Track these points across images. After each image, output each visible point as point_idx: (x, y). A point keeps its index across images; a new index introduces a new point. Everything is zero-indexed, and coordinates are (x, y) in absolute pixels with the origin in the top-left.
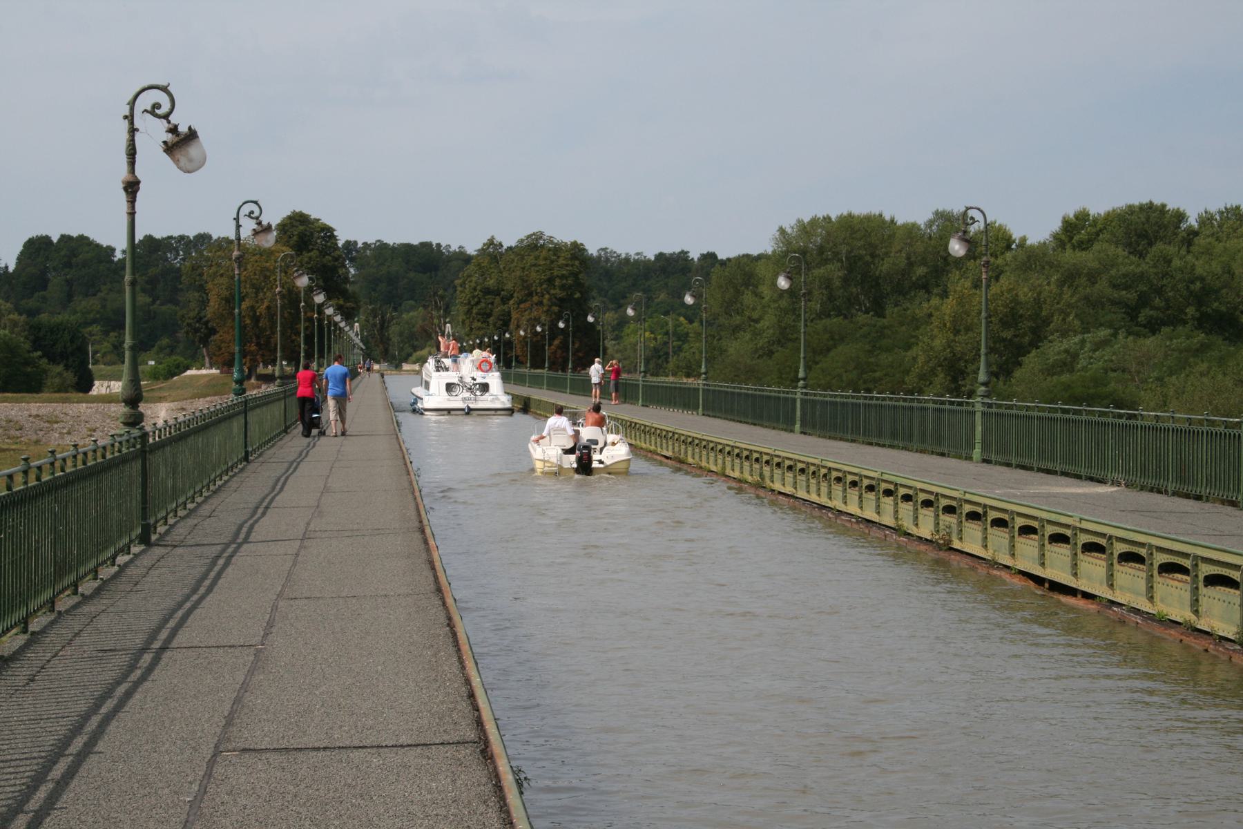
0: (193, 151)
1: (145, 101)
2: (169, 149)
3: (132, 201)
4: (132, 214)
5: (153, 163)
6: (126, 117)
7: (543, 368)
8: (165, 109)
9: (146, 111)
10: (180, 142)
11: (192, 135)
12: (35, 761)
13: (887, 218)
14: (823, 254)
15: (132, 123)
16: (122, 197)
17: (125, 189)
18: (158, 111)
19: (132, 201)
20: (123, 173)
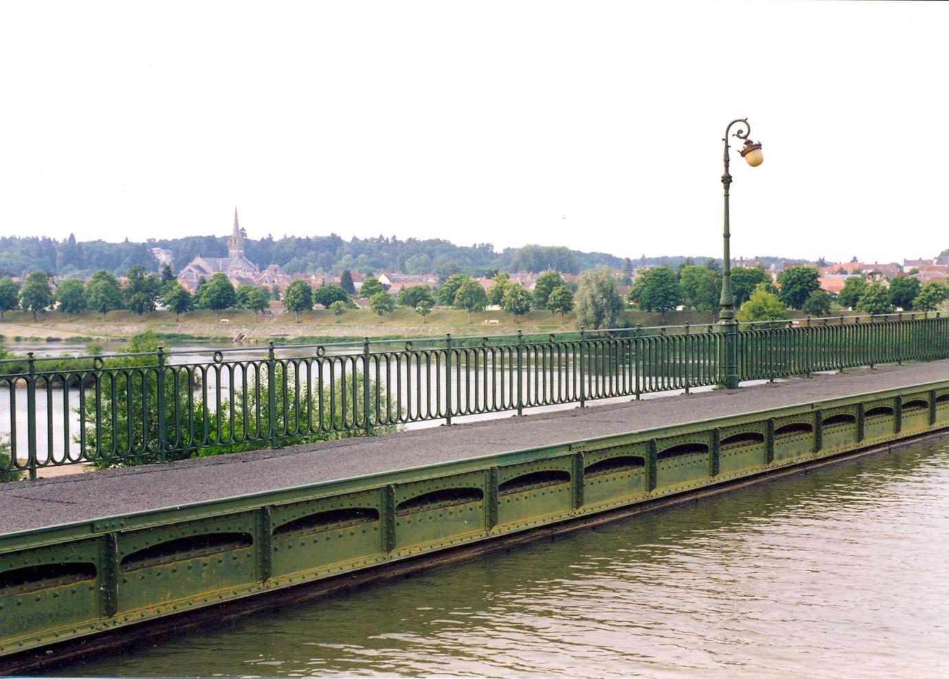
1: (734, 130)
2: (743, 154)
3: (727, 188)
4: (727, 196)
5: (739, 165)
11: (759, 146)
15: (727, 142)
19: (727, 188)
20: (723, 172)
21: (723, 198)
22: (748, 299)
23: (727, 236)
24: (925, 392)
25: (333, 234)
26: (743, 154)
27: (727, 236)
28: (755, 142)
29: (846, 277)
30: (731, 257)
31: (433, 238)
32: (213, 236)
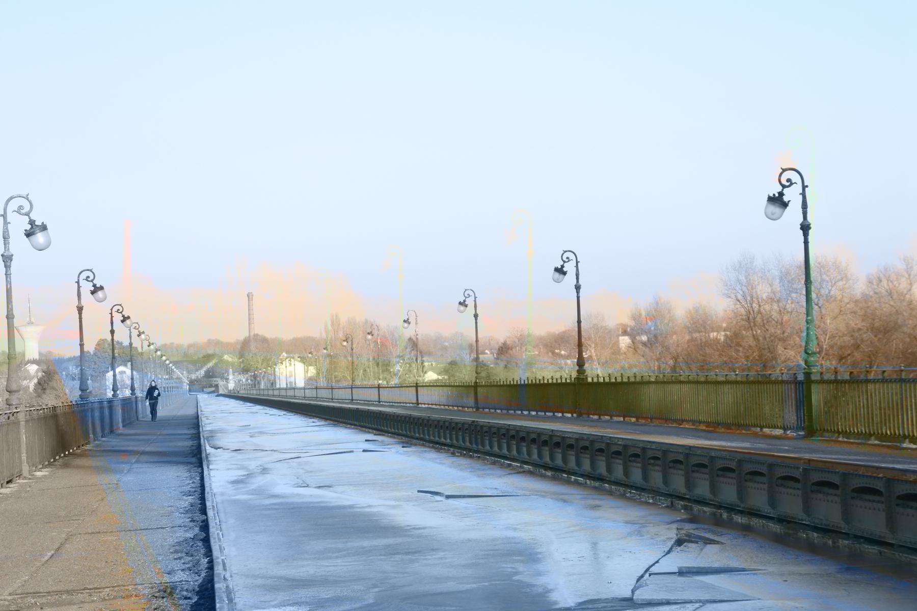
1: (115, 309)
2: (93, 293)
3: (806, 235)
8: (27, 208)
10: (96, 290)
11: (102, 288)
17: (801, 228)
20: (14, 264)
28: (565, 269)
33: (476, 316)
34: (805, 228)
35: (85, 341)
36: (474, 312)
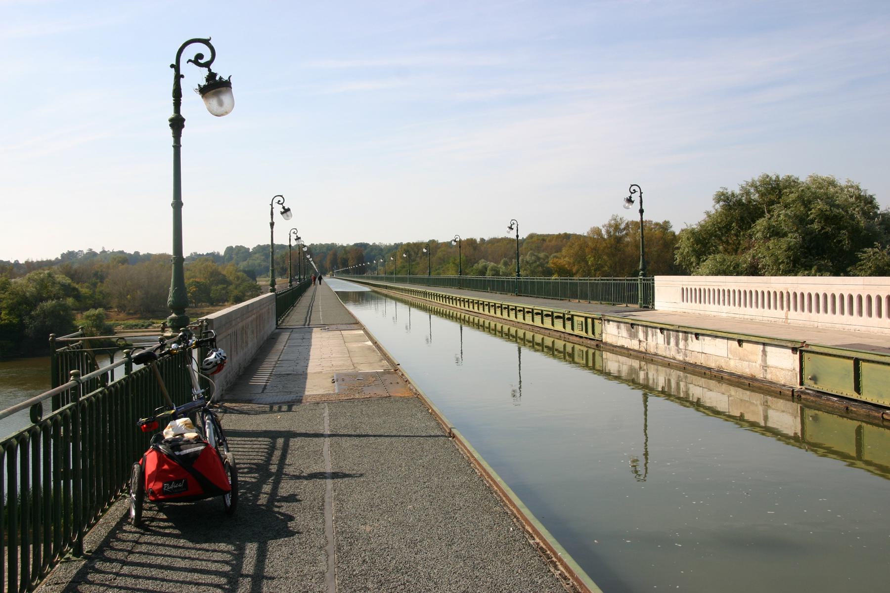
0: (225, 98)
1: (191, 52)
2: (282, 213)
3: (177, 136)
5: (194, 105)
6: (172, 66)
7: (637, 303)
8: (207, 57)
9: (190, 61)
11: (288, 210)
12: (121, 556)
13: (774, 178)
14: (535, 239)
16: (170, 132)
18: (200, 61)
19: (177, 136)
20: (171, 114)
21: (171, 151)
22: (69, 285)
23: (178, 205)
24: (849, 358)
25: (723, 197)
26: (204, 91)
27: (178, 205)
29: (784, 243)
30: (186, 254)
31: (562, 232)
32: (723, 197)
33: (641, 211)
34: (641, 211)
35: (171, 100)
36: (639, 208)
